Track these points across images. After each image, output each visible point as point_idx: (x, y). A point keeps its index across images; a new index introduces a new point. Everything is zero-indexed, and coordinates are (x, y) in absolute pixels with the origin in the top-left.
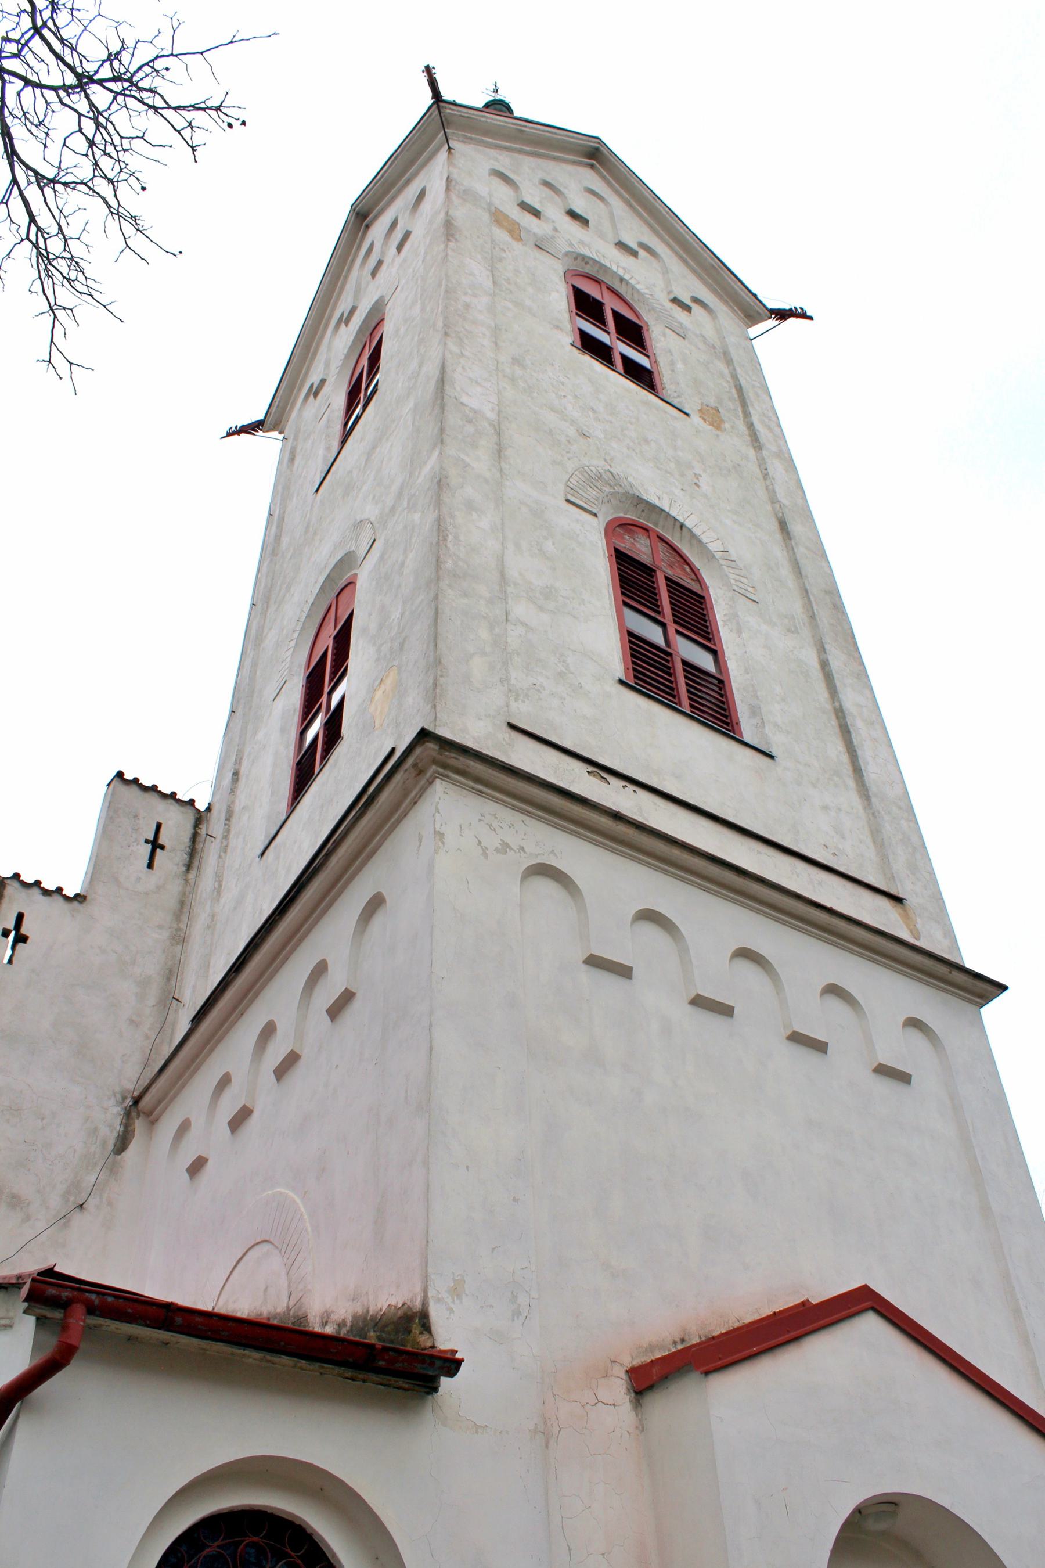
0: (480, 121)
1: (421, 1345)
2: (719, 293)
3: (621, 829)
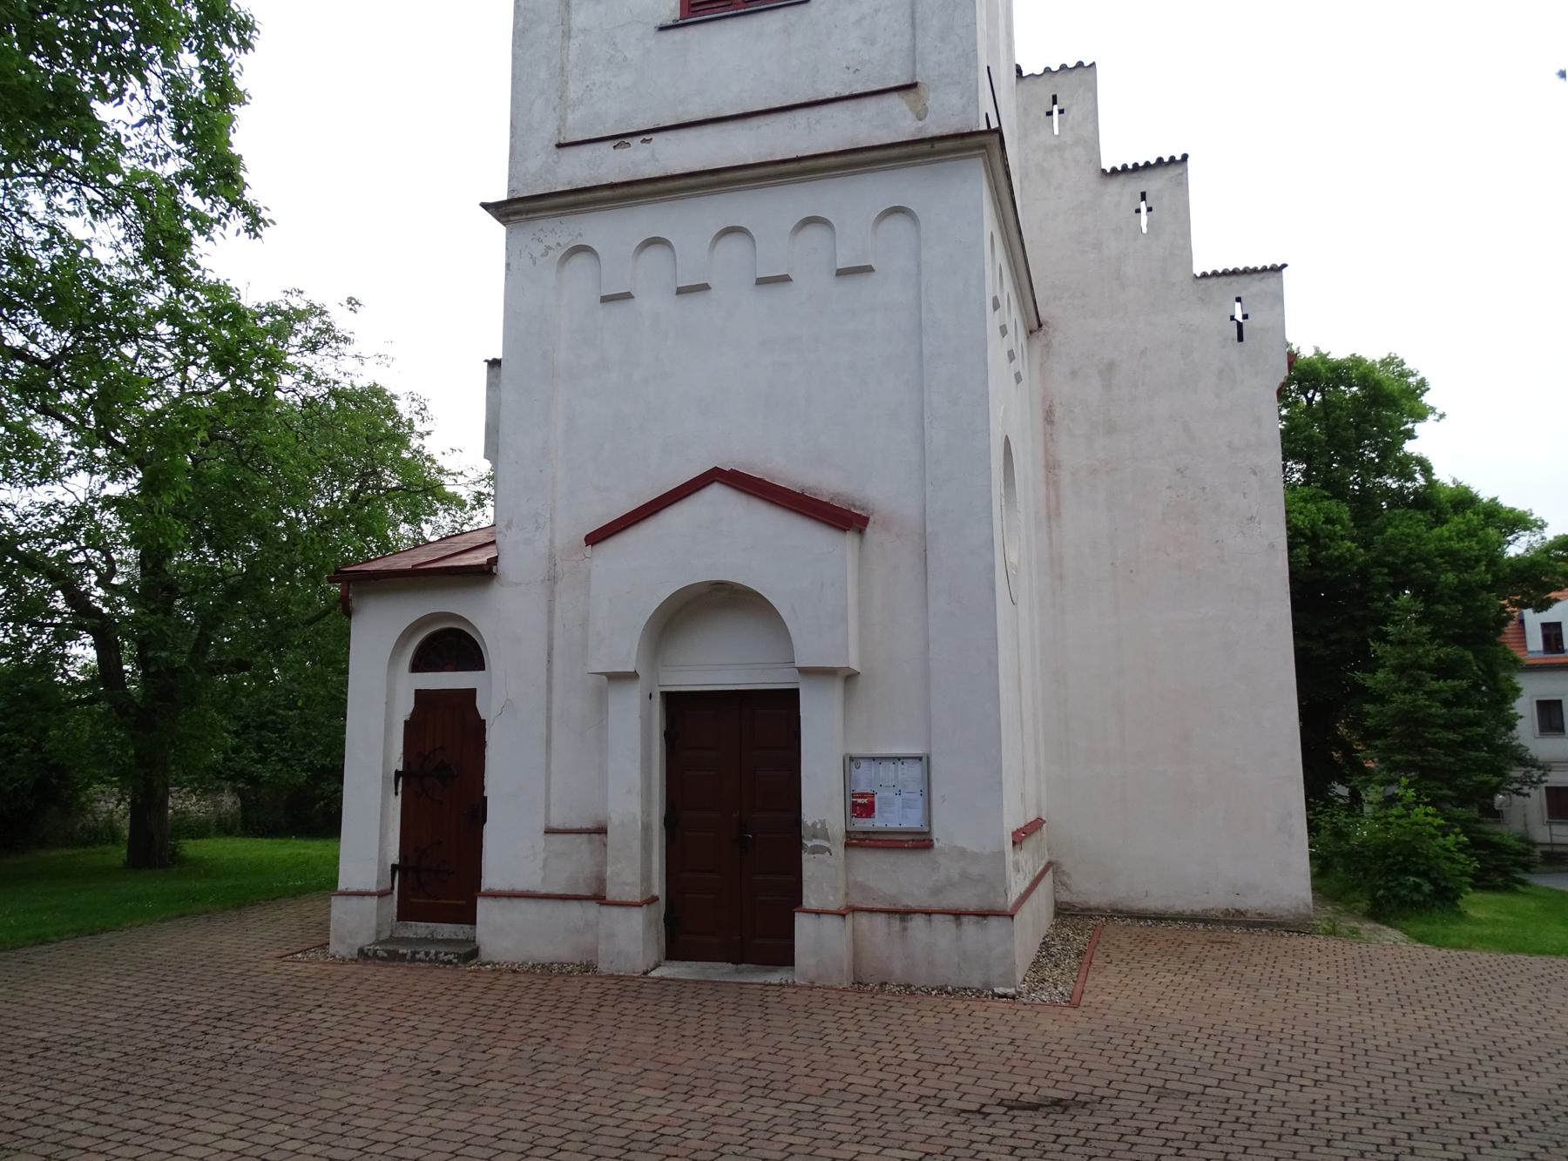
3: (619, 192)
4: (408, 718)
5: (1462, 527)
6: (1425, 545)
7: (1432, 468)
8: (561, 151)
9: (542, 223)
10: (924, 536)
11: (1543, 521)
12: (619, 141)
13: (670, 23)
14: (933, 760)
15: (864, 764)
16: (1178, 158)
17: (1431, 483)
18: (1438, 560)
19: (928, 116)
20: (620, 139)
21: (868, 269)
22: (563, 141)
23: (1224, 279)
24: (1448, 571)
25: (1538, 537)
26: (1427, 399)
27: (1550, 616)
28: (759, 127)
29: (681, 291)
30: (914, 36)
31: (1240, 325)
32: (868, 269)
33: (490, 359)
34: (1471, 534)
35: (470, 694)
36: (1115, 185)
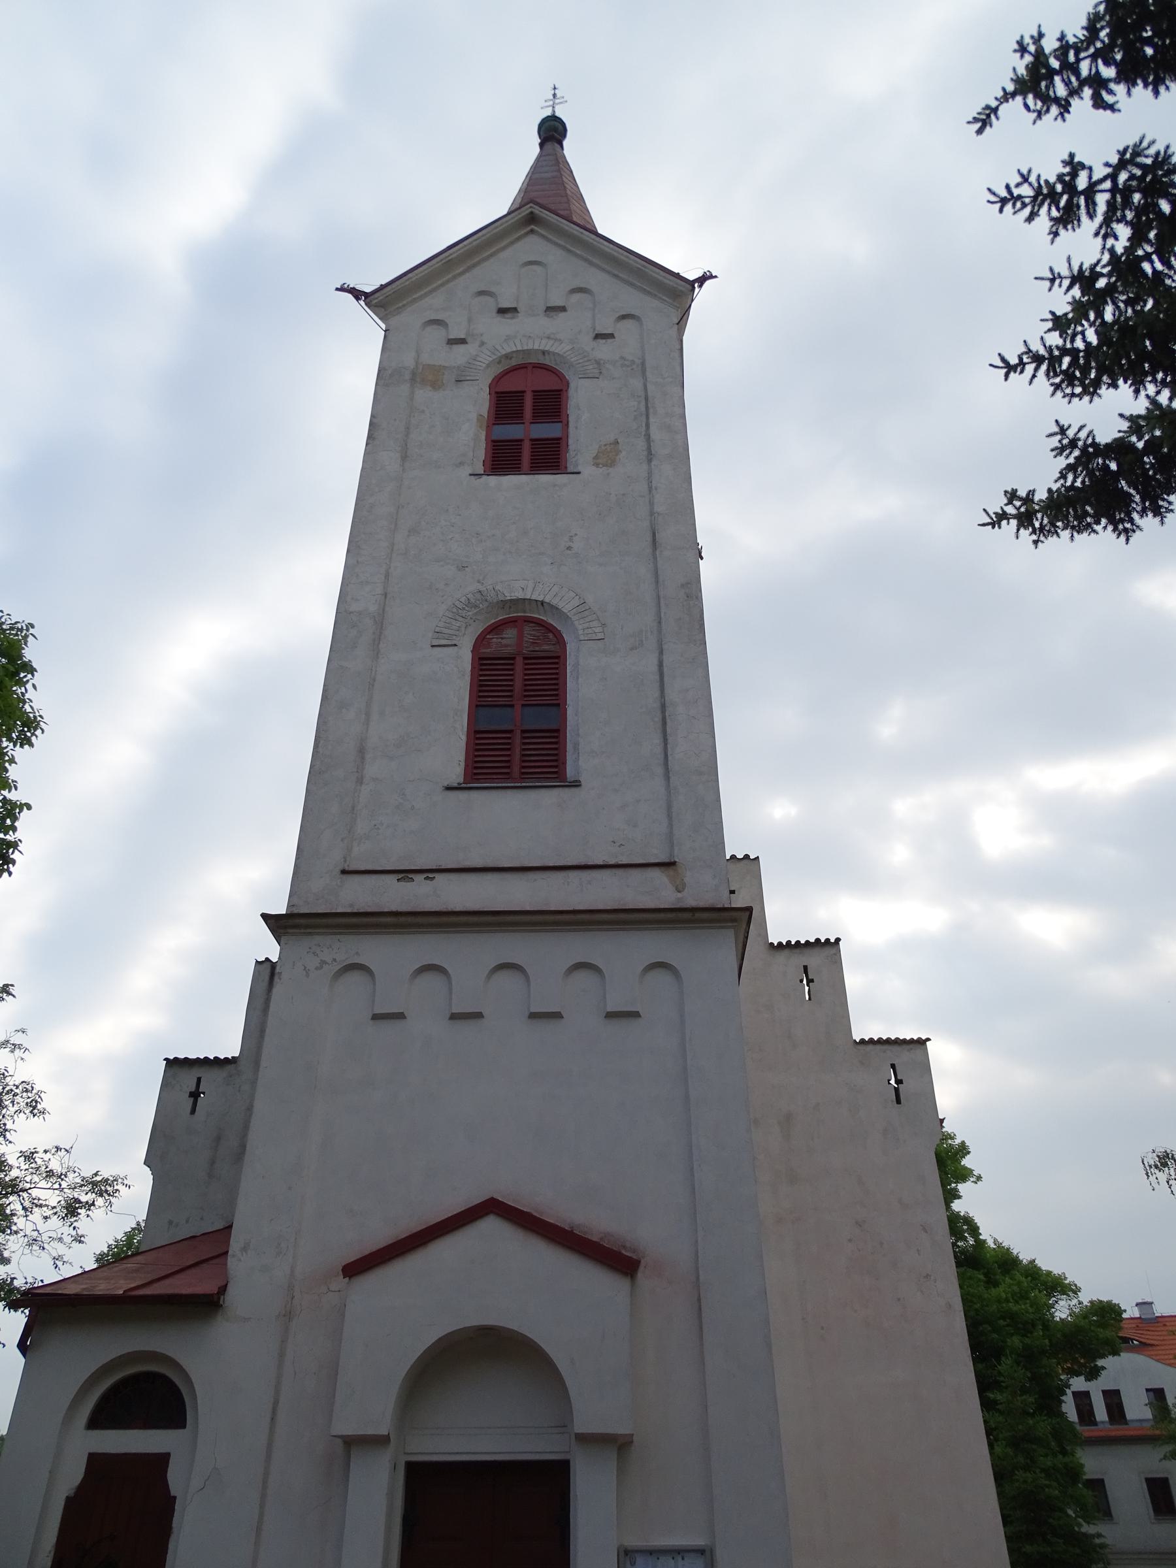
0: (406, 286)
1: (952, 1202)
2: (645, 289)
3: (402, 919)
4: (72, 1493)
5: (1015, 1288)
6: (987, 1306)
7: (978, 1228)
8: (345, 877)
9: (318, 939)
10: (697, 1284)
11: (1076, 1285)
12: (403, 875)
13: (456, 785)
14: (719, 1553)
15: (640, 1560)
16: (832, 940)
17: (981, 1244)
18: (1002, 1322)
19: (686, 890)
20: (405, 874)
21: (635, 1015)
22: (347, 868)
23: (878, 1047)
24: (1012, 1335)
25: (1075, 1301)
26: (966, 1162)
27: (1105, 1382)
28: (535, 880)
29: (454, 1017)
30: (671, 826)
31: (896, 1090)
32: (635, 1015)
33: (171, 1058)
34: (1023, 1296)
35: (162, 1460)
36: (782, 957)
